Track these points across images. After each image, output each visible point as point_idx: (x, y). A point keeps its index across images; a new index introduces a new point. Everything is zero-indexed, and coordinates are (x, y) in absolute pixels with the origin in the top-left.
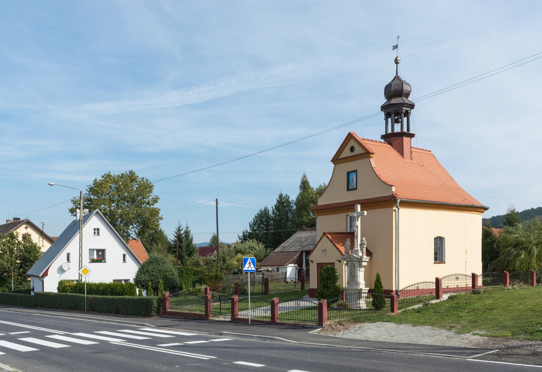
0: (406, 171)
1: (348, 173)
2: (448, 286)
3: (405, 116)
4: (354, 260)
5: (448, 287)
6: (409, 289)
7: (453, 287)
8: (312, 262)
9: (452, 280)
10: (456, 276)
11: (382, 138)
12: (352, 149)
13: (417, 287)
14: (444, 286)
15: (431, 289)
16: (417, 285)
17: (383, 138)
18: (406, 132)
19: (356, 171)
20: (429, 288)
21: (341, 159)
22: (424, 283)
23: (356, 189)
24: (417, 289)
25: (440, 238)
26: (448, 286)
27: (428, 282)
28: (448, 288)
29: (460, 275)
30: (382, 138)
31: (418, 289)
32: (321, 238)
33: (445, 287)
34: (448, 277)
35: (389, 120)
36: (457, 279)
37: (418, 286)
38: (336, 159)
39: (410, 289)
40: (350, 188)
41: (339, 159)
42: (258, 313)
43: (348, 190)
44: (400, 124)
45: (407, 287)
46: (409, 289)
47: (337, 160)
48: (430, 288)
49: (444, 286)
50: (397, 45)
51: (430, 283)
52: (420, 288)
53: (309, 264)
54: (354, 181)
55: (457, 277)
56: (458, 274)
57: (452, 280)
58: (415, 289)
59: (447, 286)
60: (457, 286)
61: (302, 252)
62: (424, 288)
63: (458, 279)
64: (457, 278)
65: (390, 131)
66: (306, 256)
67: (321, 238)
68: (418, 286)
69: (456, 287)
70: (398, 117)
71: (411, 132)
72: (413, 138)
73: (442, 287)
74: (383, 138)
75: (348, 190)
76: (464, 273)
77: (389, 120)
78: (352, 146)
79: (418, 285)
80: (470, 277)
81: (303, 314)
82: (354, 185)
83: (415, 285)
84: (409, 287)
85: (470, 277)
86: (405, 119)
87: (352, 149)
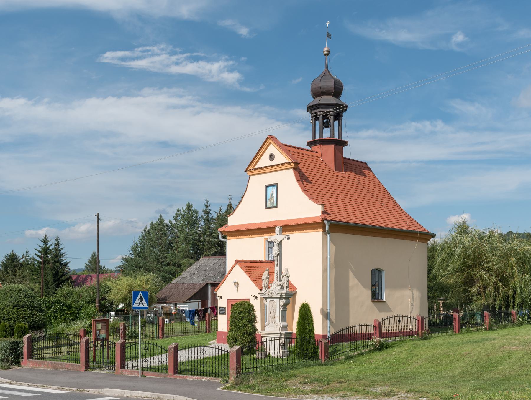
2: (388, 331)
10: (399, 318)
13: (352, 331)
14: (384, 330)
21: (257, 169)
24: (352, 333)
26: (389, 330)
37: (353, 330)
39: (346, 333)
48: (369, 332)
49: (384, 330)
52: (355, 333)
55: (400, 319)
58: (350, 333)
59: (387, 330)
62: (361, 333)
68: (353, 330)
73: (382, 332)
79: (353, 329)
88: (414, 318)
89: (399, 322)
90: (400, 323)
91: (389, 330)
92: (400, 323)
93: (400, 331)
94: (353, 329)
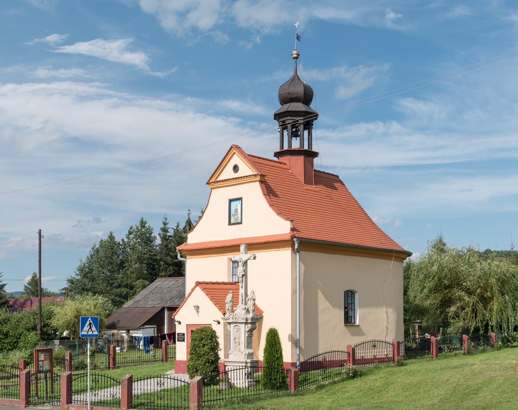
2: (362, 357)
5: (376, 357)
6: (313, 361)
7: (381, 357)
10: (373, 343)
12: (236, 168)
13: (323, 358)
24: (323, 360)
37: (324, 357)
46: (313, 361)
48: (342, 359)
52: (327, 360)
58: (321, 360)
60: (375, 356)
68: (324, 357)
73: (356, 358)
78: (236, 164)
79: (325, 356)
84: (313, 359)
89: (374, 348)
90: (374, 349)
92: (374, 349)
93: (375, 357)
94: (325, 356)
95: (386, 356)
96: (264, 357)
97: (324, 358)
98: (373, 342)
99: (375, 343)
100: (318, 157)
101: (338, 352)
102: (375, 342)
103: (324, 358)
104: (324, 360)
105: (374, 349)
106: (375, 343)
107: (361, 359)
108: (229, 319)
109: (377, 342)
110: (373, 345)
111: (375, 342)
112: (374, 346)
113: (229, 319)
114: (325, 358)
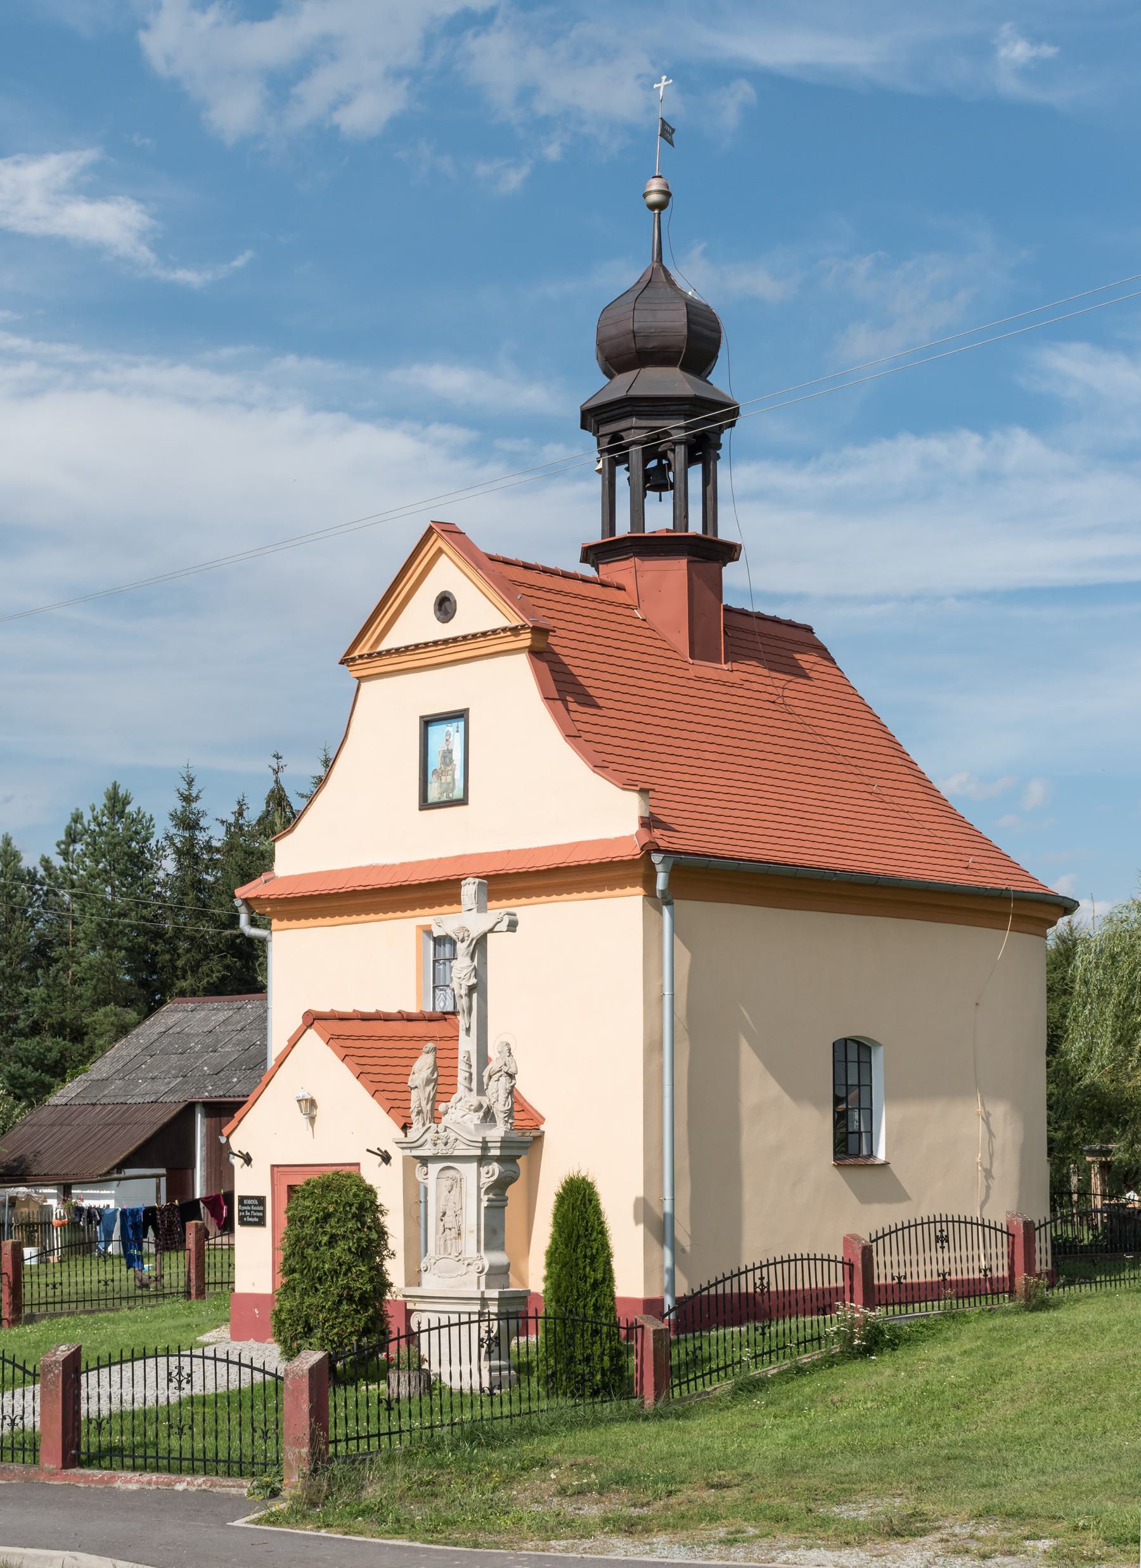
0: (692, 727)
1: (427, 722)
2: (899, 1278)
3: (691, 460)
4: (456, 1153)
5: (947, 1277)
6: (728, 1291)
8: (248, 1159)
9: (455, 1359)
10: (938, 1228)
11: (584, 559)
12: (445, 606)
13: (758, 1282)
15: (830, 1290)
16: (758, 1272)
17: (591, 558)
18: (700, 532)
19: (461, 715)
20: (813, 1286)
21: (388, 652)
22: (812, 1262)
23: (463, 801)
24: (758, 1290)
25: (859, 1043)
26: (902, 1274)
27: (812, 1256)
28: (903, 1287)
29: (956, 1224)
30: (584, 559)
31: (764, 1289)
32: (293, 1042)
33: (977, 1276)
34: (906, 1231)
35: (622, 475)
36: (939, 1245)
38: (366, 651)
40: (433, 795)
41: (380, 654)
42: (212, 1257)
43: (425, 804)
44: (668, 495)
45: (713, 1281)
46: (728, 1291)
47: (370, 656)
50: (341, 663)
51: (819, 1263)
52: (773, 1288)
53: (231, 1168)
54: (451, 761)
55: (942, 1231)
56: (944, 1219)
57: (455, 1359)
58: (751, 1290)
59: (941, 1271)
60: (944, 1275)
61: (190, 1109)
63: (945, 1244)
64: (942, 1239)
65: (623, 528)
66: (214, 1134)
67: (293, 1042)
68: (762, 1279)
69: (935, 1278)
70: (660, 462)
71: (726, 533)
72: (729, 564)
73: (876, 1282)
74: (591, 558)
75: (425, 804)
76: (974, 1212)
77: (622, 475)
79: (765, 1275)
80: (1002, 1232)
81: (235, 1416)
82: (453, 779)
83: (750, 1274)
84: (720, 1286)
85: (1002, 1232)
86: (695, 474)
87: (445, 606)
88: (999, 1227)
89: (939, 1245)
90: (943, 1248)
91: (902, 1274)
92: (943, 1248)
95: (986, 1275)
96: (546, 1279)
97: (762, 1284)
98: (938, 1225)
99: (944, 1227)
100: (737, 559)
101: (812, 1262)
102: (944, 1224)
103: (762, 1284)
104: (762, 1290)
105: (940, 1250)
106: (944, 1227)
107: (893, 1286)
108: (421, 1146)
109: (950, 1224)
110: (939, 1234)
111: (944, 1224)
112: (942, 1239)
113: (421, 1146)
114: (765, 1282)
